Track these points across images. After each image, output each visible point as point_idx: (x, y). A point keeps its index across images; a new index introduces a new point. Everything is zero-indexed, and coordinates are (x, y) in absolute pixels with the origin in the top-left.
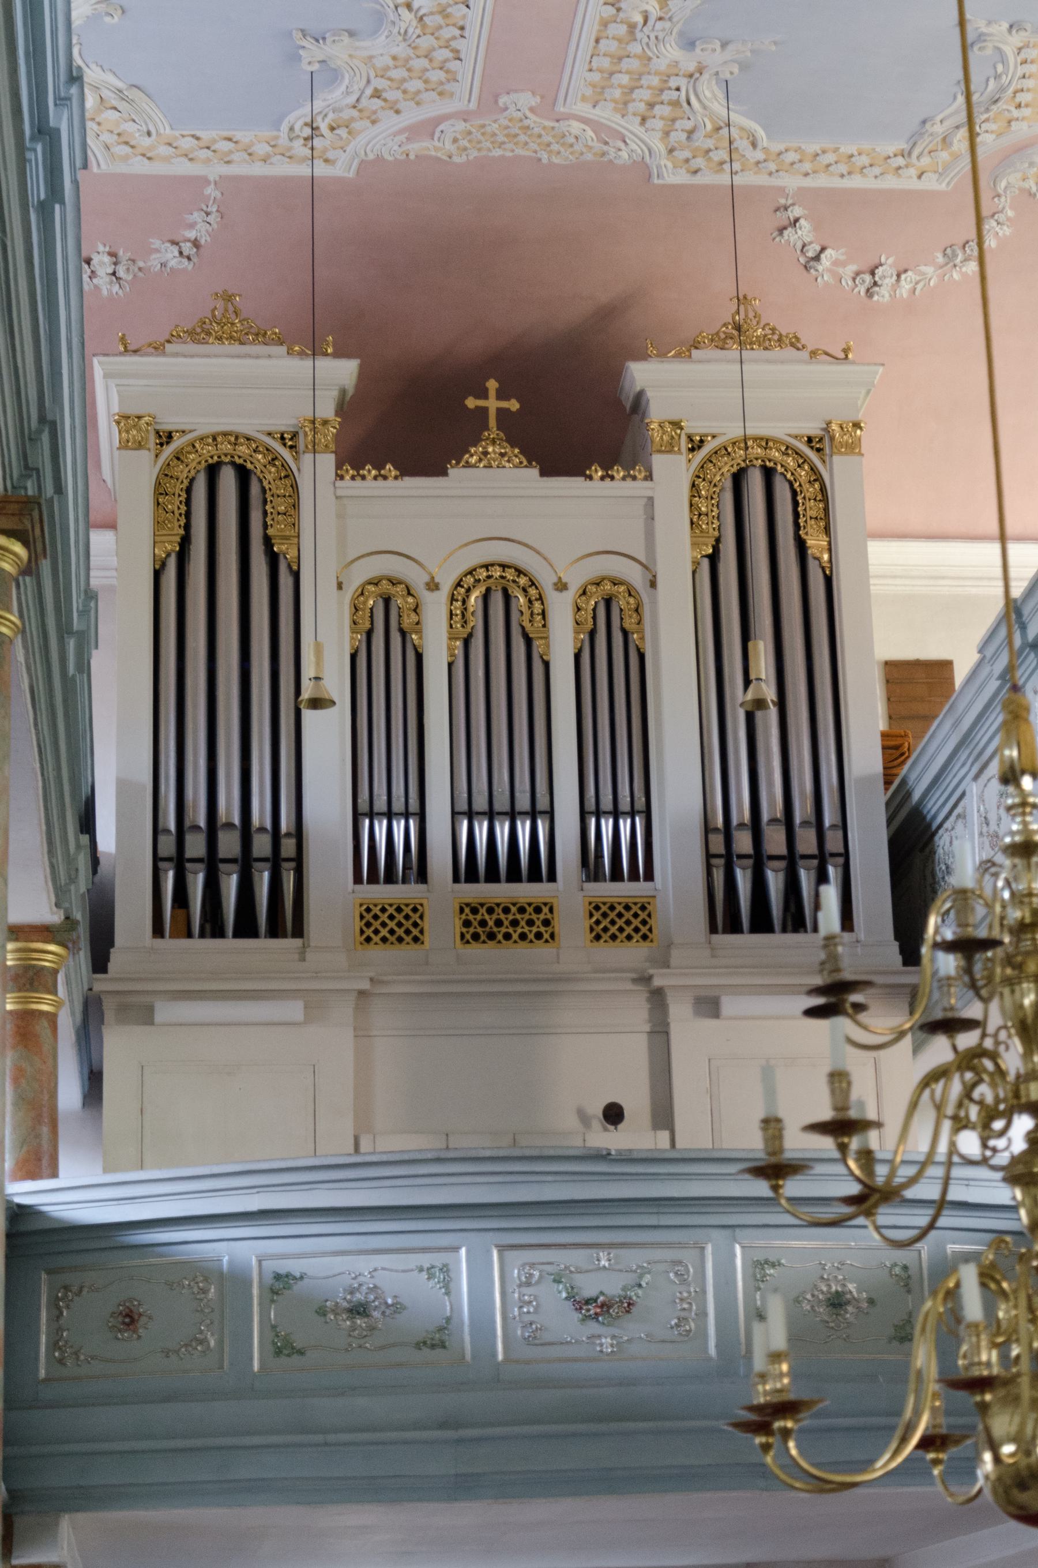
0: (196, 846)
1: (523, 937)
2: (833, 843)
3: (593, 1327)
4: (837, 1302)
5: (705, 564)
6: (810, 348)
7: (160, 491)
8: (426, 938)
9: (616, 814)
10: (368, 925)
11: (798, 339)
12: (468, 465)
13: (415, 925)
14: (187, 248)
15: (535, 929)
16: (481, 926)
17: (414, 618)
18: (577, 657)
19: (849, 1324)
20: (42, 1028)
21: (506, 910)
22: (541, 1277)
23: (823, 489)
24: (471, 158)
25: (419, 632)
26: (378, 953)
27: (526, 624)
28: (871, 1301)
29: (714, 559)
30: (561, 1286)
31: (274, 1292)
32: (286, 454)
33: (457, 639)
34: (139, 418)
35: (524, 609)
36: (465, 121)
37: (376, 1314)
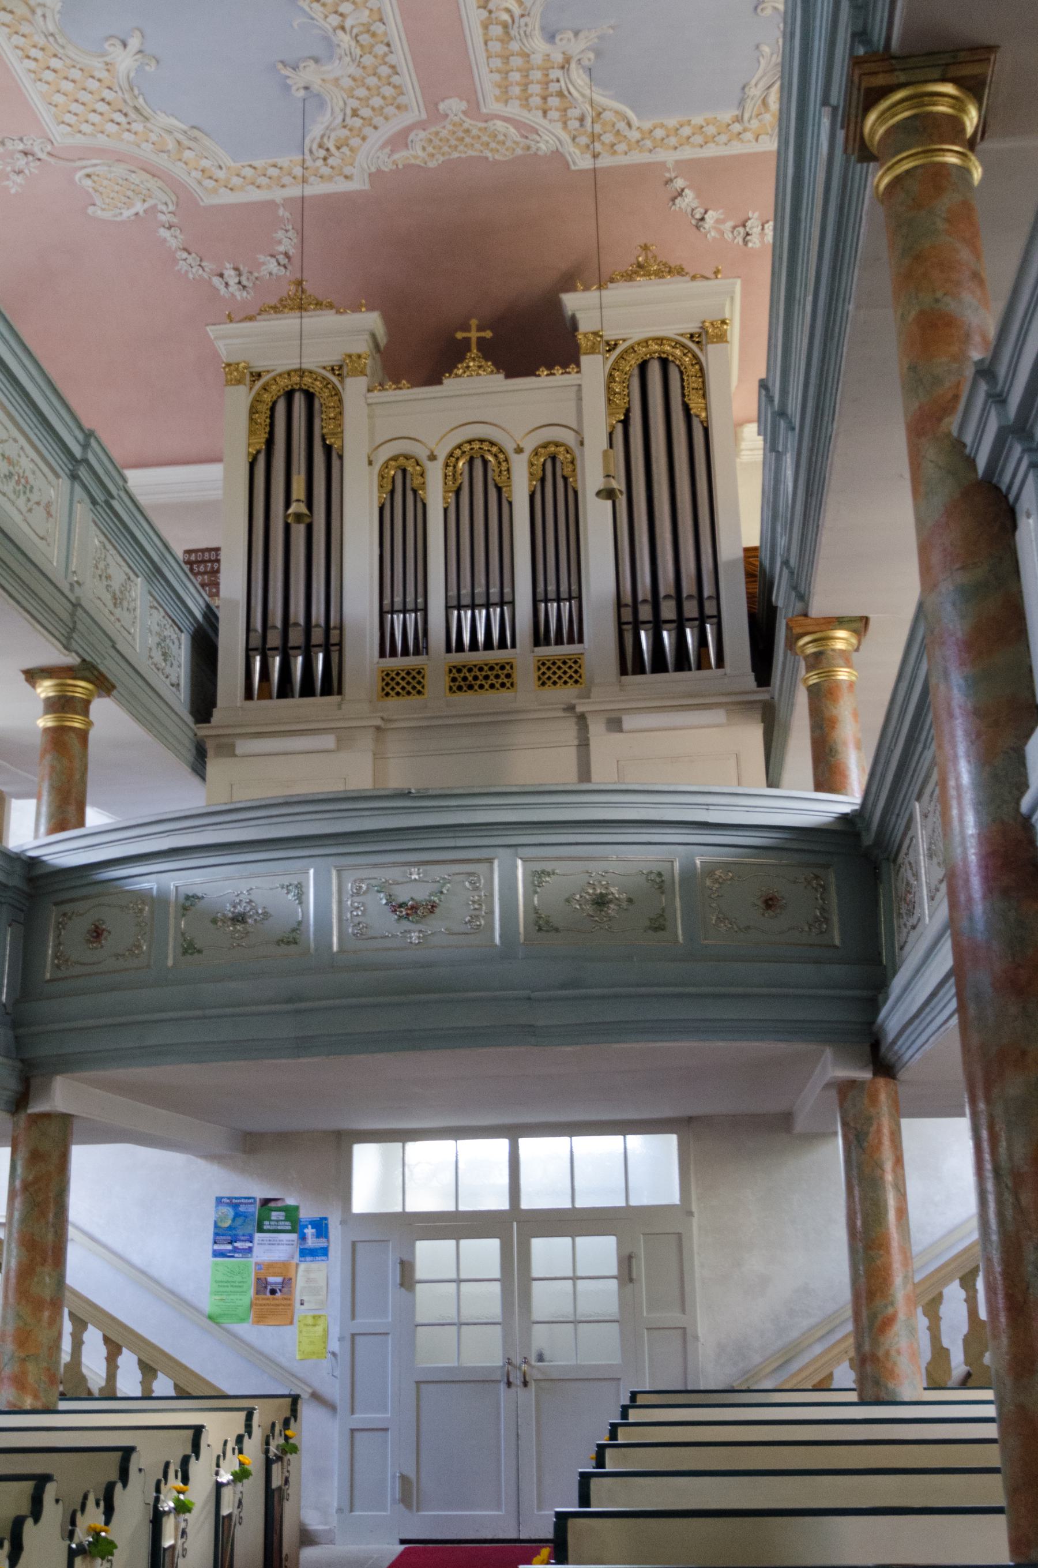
0: (274, 639)
1: (492, 686)
2: (710, 609)
3: (406, 925)
4: (601, 902)
5: (620, 428)
6: (692, 274)
7: (253, 411)
8: (425, 691)
9: (559, 600)
10: (387, 684)
11: (682, 269)
12: (457, 376)
13: (419, 683)
14: (281, 258)
15: (500, 681)
16: (464, 680)
17: (420, 480)
18: (532, 497)
19: (611, 919)
20: (74, 741)
21: (481, 669)
22: (368, 888)
23: (702, 369)
24: (440, 162)
25: (423, 489)
26: (393, 702)
27: (497, 478)
28: (630, 901)
29: (626, 423)
30: (382, 895)
31: (185, 908)
32: (335, 379)
33: (450, 491)
34: (238, 364)
35: (496, 468)
36: (424, 130)
37: (250, 921)
